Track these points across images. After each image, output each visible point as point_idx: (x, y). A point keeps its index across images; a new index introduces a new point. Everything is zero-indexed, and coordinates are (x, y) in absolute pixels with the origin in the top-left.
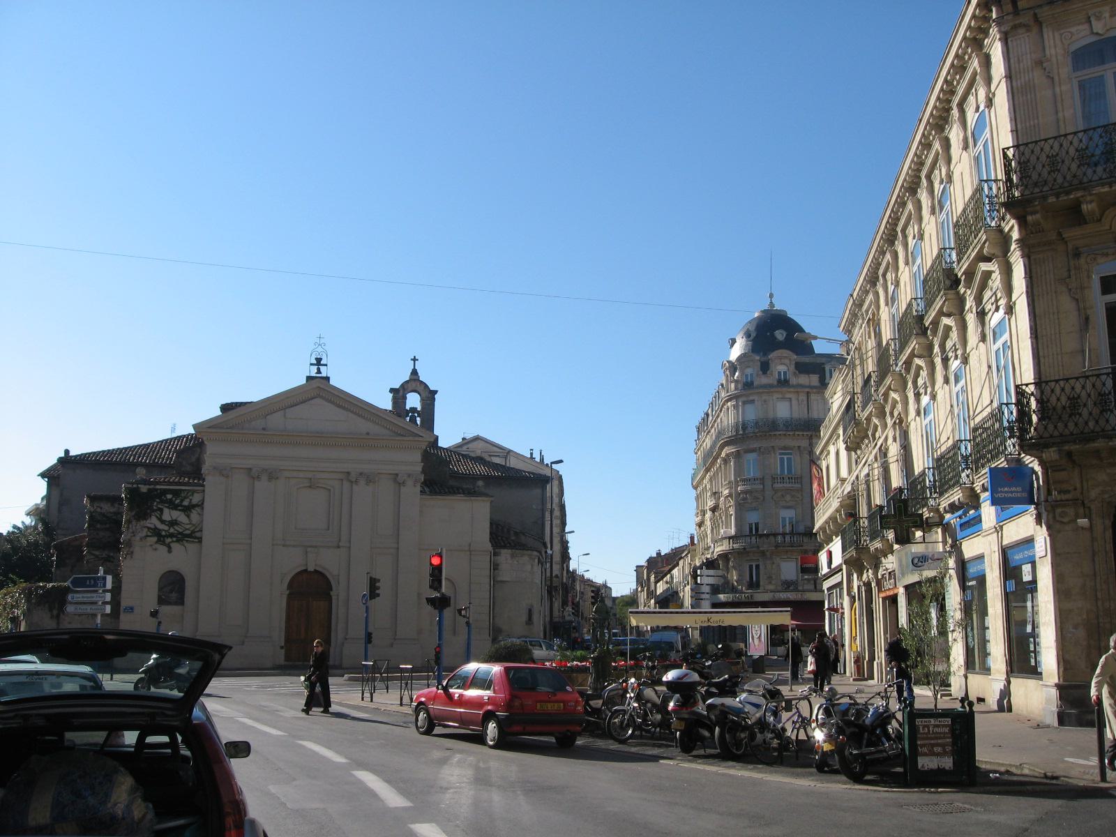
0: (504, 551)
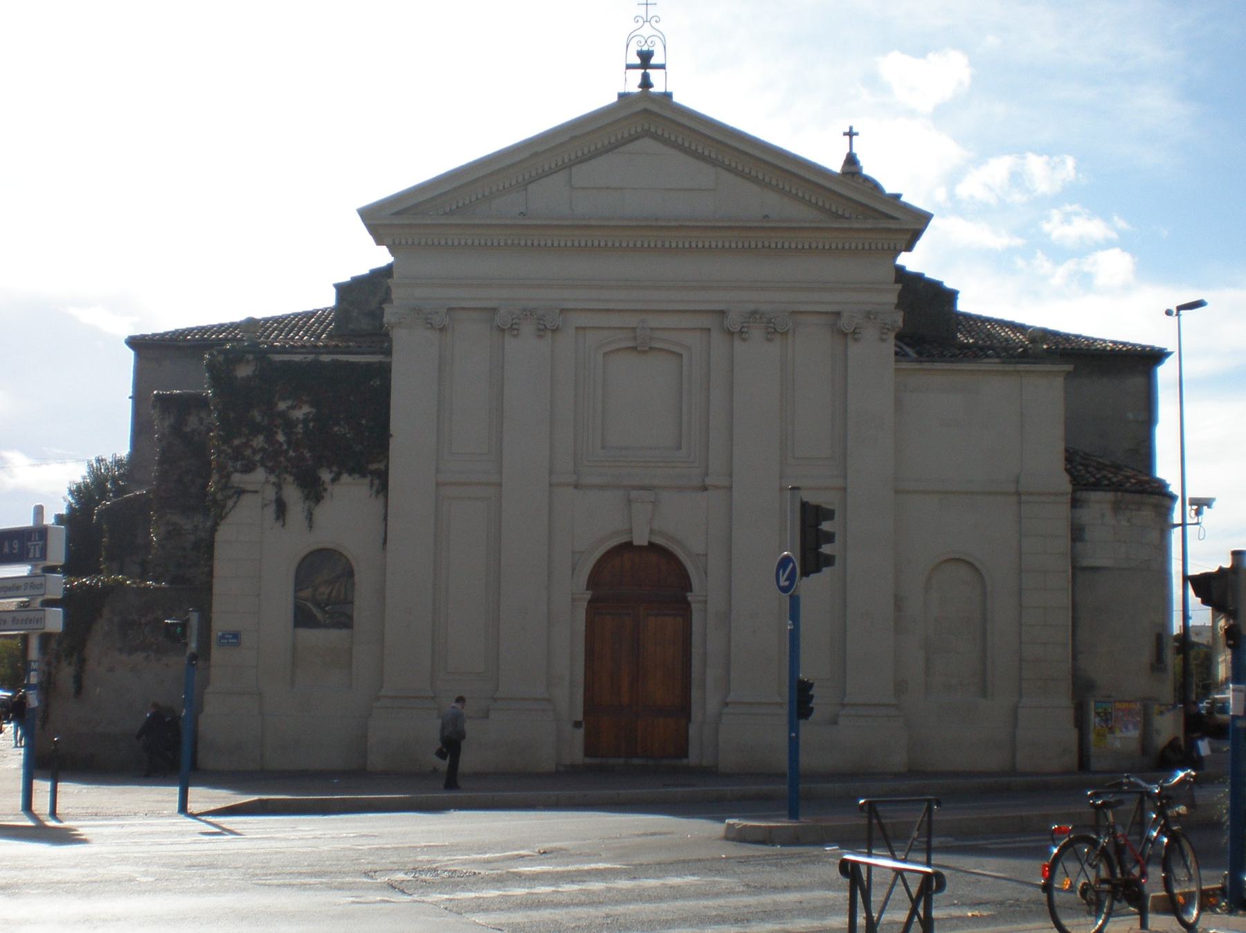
0: (1094, 496)
